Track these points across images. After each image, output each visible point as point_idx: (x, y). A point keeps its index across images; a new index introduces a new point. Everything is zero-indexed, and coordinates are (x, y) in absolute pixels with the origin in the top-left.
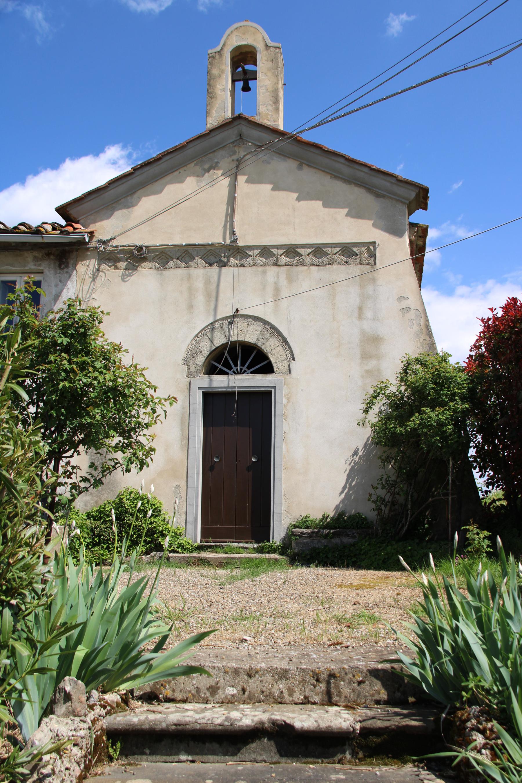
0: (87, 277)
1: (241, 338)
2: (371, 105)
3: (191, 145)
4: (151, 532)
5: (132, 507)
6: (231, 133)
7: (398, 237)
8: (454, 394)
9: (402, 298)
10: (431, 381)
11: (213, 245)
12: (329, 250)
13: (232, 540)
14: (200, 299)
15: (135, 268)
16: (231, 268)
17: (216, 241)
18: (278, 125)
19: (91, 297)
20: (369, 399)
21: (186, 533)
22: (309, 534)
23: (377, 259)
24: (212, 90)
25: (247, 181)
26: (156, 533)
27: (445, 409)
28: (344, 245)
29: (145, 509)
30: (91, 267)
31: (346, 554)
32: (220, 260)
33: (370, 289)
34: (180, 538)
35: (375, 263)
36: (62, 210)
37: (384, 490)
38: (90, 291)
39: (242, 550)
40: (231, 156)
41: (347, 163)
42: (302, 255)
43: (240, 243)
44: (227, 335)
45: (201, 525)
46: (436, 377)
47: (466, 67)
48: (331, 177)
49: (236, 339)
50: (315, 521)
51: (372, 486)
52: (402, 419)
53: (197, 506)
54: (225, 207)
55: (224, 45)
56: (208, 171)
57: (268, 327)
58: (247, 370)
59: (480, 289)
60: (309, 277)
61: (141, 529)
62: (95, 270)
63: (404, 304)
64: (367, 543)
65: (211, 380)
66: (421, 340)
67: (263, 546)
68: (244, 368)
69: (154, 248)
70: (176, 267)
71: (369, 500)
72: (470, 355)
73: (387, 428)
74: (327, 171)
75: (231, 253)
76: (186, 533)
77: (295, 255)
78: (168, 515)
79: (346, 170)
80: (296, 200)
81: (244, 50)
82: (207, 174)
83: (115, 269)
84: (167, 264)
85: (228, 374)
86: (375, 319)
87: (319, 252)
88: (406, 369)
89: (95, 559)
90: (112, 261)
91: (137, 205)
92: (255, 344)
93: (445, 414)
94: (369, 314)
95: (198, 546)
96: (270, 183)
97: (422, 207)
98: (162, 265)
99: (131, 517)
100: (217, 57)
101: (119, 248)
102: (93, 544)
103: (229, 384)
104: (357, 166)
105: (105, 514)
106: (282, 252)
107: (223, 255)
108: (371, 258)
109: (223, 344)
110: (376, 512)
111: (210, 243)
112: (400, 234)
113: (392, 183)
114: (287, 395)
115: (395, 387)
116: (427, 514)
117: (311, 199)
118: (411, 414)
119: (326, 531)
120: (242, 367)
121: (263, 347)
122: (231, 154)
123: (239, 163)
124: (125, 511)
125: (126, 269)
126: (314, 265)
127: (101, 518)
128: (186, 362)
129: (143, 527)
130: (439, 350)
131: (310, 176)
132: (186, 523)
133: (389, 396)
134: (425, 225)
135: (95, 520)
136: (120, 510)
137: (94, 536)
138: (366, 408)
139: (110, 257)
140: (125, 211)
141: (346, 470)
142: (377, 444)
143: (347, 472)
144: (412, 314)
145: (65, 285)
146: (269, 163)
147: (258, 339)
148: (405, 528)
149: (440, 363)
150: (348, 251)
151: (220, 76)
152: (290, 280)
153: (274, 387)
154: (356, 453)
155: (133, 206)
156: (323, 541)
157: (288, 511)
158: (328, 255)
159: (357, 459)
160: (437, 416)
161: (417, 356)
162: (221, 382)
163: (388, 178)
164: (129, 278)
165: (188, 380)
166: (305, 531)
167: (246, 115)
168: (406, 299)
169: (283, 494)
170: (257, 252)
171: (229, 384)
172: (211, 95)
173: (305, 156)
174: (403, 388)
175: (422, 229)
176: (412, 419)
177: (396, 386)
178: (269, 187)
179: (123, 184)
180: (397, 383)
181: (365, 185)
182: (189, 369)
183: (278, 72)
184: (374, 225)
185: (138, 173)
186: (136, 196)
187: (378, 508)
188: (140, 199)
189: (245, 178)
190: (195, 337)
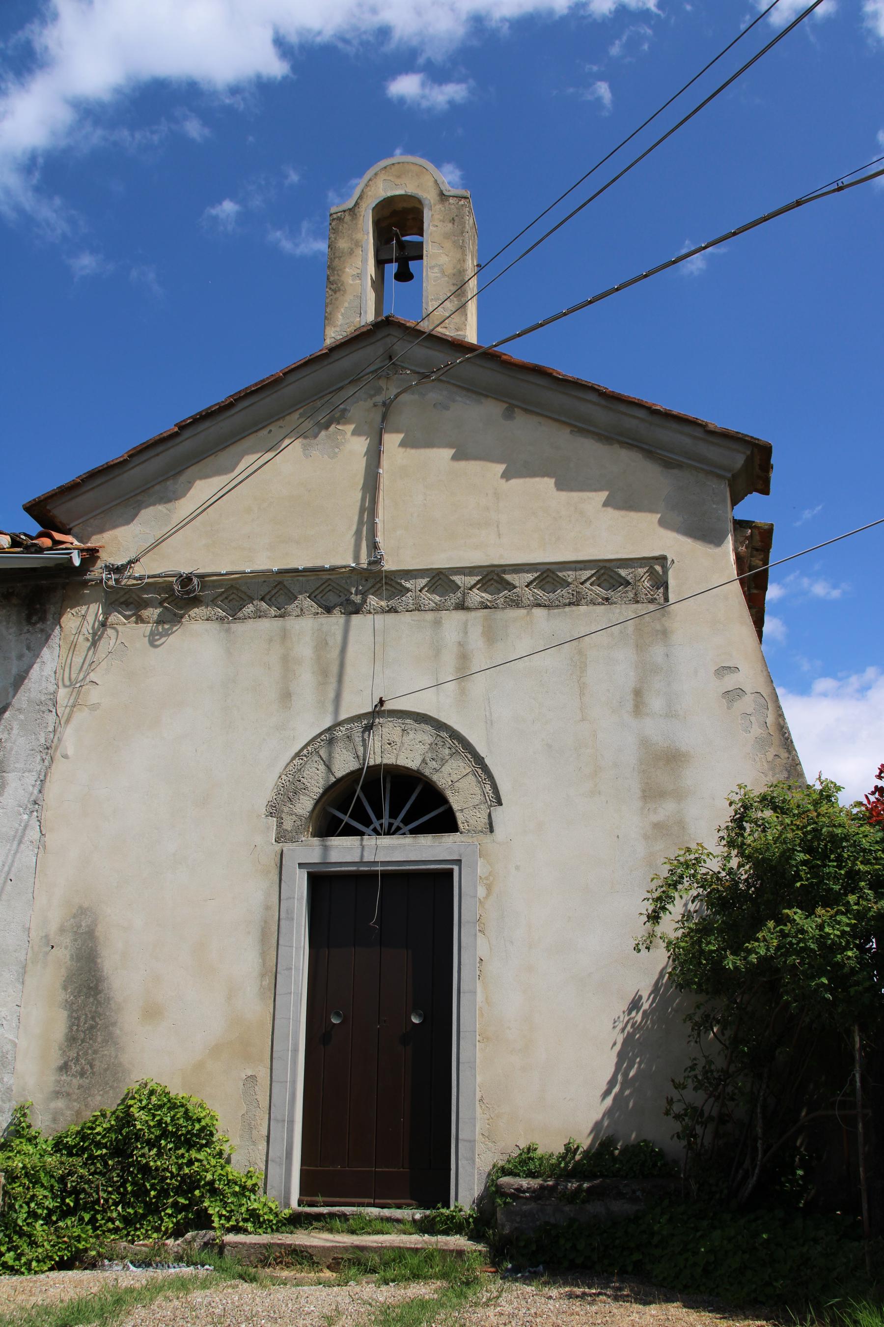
0: (81, 638)
1: (389, 759)
2: (646, 276)
3: (292, 378)
4: (189, 1184)
5: (149, 1127)
6: (371, 352)
7: (711, 546)
8: (853, 876)
9: (724, 671)
10: (800, 845)
11: (333, 569)
12: (570, 576)
13: (366, 1200)
14: (306, 680)
15: (176, 619)
16: (371, 616)
17: (338, 561)
18: (465, 336)
19: (88, 680)
20: (660, 890)
21: (265, 1184)
22: (534, 1191)
23: (670, 590)
24: (336, 277)
25: (403, 444)
26: (198, 1187)
27: (838, 912)
28: (601, 564)
29: (178, 1130)
30: (90, 618)
31: (617, 1242)
32: (347, 600)
33: (657, 652)
34: (253, 1197)
35: (666, 599)
36: (37, 509)
37: (700, 1092)
38: (86, 666)
39: (387, 1226)
40: (371, 397)
41: (603, 402)
42: (515, 587)
43: (389, 565)
44: (361, 753)
45: (302, 1165)
46: (809, 837)
47: (840, 185)
48: (572, 432)
49: (378, 762)
50: (548, 1160)
51: (673, 1081)
52: (738, 934)
53: (291, 1122)
54: (359, 495)
55: (361, 197)
56: (327, 427)
57: (444, 734)
58: (401, 825)
59: (854, 681)
60: (531, 629)
61: (167, 1178)
62: (97, 623)
63: (730, 682)
64: (666, 1217)
65: (326, 849)
66: (770, 757)
67: (435, 1217)
68: (397, 823)
69: (215, 578)
70: (259, 615)
71: (667, 1113)
72: (876, 787)
73: (702, 952)
74: (563, 419)
75: (369, 585)
76: (265, 1184)
77: (499, 586)
78: (228, 1144)
79: (601, 415)
80: (502, 477)
81: (400, 206)
82: (323, 433)
83: (136, 623)
84: (241, 609)
85: (361, 834)
86: (670, 714)
87: (549, 579)
88: (741, 819)
89: (59, 1250)
90: (132, 606)
91: (184, 495)
92: (418, 772)
93: (839, 923)
94: (656, 704)
95: (291, 1215)
96: (450, 446)
97: (760, 487)
98: (231, 612)
99: (146, 1150)
100: (347, 218)
101: (146, 581)
102: (62, 1211)
103: (362, 856)
104: (623, 408)
105: (93, 1141)
106: (473, 582)
107: (353, 590)
108: (658, 588)
109: (352, 773)
110: (684, 1143)
111: (327, 566)
112: (716, 540)
113: (695, 438)
114: (486, 878)
115: (716, 859)
116: (798, 1143)
117: (533, 475)
118: (758, 923)
119: (572, 1185)
120: (392, 821)
121: (435, 778)
122: (372, 392)
123: (387, 410)
124: (136, 1134)
125: (160, 622)
126: (539, 605)
127: (84, 1150)
128: (274, 811)
129: (171, 1172)
130: (811, 778)
131: (527, 430)
132: (267, 1161)
133: (706, 880)
134: (767, 525)
135: (70, 1154)
136: (124, 1132)
137: (65, 1192)
138: (654, 911)
139: (128, 597)
140: (160, 508)
141: (615, 1044)
142: (680, 986)
143: (618, 1047)
144: (747, 703)
145: (37, 656)
146: (447, 408)
147: (424, 761)
148: (752, 1182)
149: (816, 804)
150: (609, 576)
151: (351, 252)
152: (491, 636)
153: (458, 862)
154: (635, 1005)
155: (177, 498)
156: (567, 1209)
157: (488, 1136)
158: (569, 584)
159: (639, 1018)
160: (821, 927)
161: (763, 790)
162: (345, 851)
163: (688, 429)
164: (163, 639)
165: (278, 847)
166: (525, 1183)
167: (400, 318)
168: (734, 672)
169: (478, 1097)
170: (423, 582)
171: (362, 856)
172: (333, 287)
173: (521, 394)
174: (734, 863)
175: (760, 533)
176: (760, 935)
177: (720, 858)
178: (449, 453)
179: (157, 455)
180: (722, 850)
181: (639, 444)
182: (280, 824)
183: (463, 241)
184: (662, 523)
185: (187, 434)
186: (183, 478)
187: (688, 1134)
188: (190, 484)
189: (398, 437)
190: (293, 758)
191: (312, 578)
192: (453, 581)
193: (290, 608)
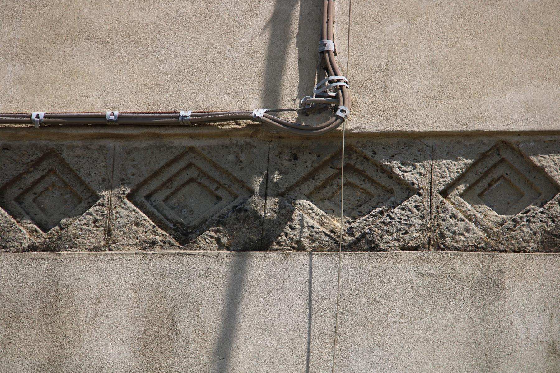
11: (202, 122)
16: (301, 258)
17: (219, 102)
43: (360, 117)
75: (301, 170)
107: (257, 184)
111: (186, 113)
191: (144, 144)
192: (541, 170)
193: (75, 225)
